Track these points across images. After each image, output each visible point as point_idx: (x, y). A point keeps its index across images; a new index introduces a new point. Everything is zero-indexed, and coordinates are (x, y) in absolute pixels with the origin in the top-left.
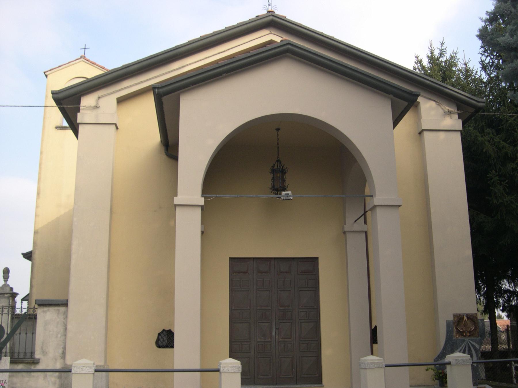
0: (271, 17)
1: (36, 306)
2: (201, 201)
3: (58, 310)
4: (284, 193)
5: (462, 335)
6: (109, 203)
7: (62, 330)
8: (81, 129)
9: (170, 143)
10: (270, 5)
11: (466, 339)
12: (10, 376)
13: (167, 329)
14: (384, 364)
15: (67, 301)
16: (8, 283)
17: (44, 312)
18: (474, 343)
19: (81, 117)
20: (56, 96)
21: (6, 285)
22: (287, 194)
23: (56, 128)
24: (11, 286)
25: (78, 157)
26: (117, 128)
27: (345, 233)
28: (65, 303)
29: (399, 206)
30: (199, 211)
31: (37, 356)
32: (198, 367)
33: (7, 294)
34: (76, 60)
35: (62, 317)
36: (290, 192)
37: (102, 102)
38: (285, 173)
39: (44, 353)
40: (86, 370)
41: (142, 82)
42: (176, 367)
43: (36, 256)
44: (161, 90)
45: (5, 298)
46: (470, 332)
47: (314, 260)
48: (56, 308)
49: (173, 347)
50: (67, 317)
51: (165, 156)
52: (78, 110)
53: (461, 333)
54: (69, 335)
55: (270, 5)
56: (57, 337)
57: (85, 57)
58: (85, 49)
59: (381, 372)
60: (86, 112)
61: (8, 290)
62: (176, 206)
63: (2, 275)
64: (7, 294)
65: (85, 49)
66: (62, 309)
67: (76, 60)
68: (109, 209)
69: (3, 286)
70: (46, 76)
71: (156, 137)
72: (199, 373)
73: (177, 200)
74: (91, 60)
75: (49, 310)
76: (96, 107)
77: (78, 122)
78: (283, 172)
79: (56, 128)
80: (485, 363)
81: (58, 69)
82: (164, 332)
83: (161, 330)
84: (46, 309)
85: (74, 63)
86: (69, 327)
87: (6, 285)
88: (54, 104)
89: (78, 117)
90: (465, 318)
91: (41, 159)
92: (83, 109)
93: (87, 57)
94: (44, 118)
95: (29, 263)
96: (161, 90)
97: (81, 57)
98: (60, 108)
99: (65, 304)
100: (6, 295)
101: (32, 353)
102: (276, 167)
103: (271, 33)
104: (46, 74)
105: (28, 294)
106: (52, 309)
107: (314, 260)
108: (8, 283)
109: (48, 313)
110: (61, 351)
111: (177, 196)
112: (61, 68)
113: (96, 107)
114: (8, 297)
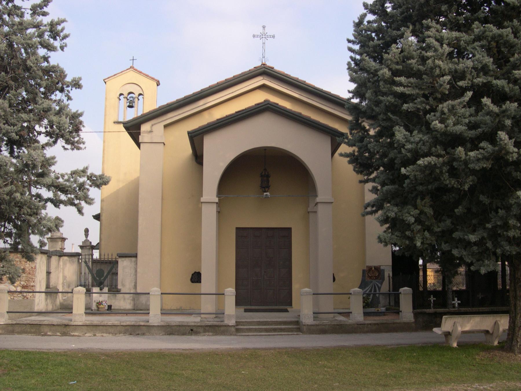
0: (264, 69)
1: (117, 257)
2: (217, 200)
3: (131, 260)
4: (265, 193)
5: (371, 278)
6: (161, 194)
7: (134, 272)
8: (141, 145)
9: (198, 154)
10: (264, 57)
11: (374, 281)
12: (108, 297)
13: (197, 271)
14: (312, 293)
15: (137, 254)
16: (88, 238)
17: (122, 261)
18: (377, 283)
19: (141, 139)
20: (126, 125)
21: (87, 241)
22: (267, 195)
23: (114, 123)
24: (90, 241)
25: (141, 165)
26: (164, 144)
27: (308, 212)
28: (135, 255)
29: (332, 203)
30: (215, 206)
31: (119, 287)
32: (214, 292)
33: (88, 246)
34: (127, 70)
35: (133, 264)
36: (268, 193)
37: (154, 128)
38: (269, 177)
39: (123, 285)
40: (157, 293)
41: (180, 114)
42: (202, 292)
43: (103, 218)
44: (192, 134)
45: (87, 249)
46: (375, 277)
47: (289, 229)
48: (130, 258)
49: (200, 282)
50: (137, 264)
51: (195, 163)
52: (139, 134)
53: (370, 277)
54: (138, 275)
55: (264, 57)
56: (131, 276)
57: (133, 67)
58: (133, 60)
59: (311, 297)
60: (144, 135)
61: (88, 244)
62: (202, 203)
63: (84, 233)
64: (88, 246)
65: (133, 60)
66: (133, 259)
67: (127, 70)
68: (161, 198)
69: (85, 241)
70: (105, 83)
71: (189, 150)
72: (215, 295)
73: (203, 199)
74: (139, 69)
75: (125, 260)
76: (151, 131)
77: (140, 141)
78: (268, 176)
79: (114, 123)
80: (394, 293)
81: (114, 77)
82: (196, 274)
83: (194, 272)
84: (123, 259)
85: (125, 72)
86: (138, 270)
87: (87, 241)
88: (124, 130)
89: (140, 138)
90: (373, 268)
91: (104, 146)
92: (143, 133)
93: (135, 67)
94: (105, 115)
95: (98, 223)
96: (192, 134)
97: (131, 68)
98: (128, 133)
99: (136, 256)
100: (87, 247)
101: (116, 285)
102: (263, 174)
103: (264, 79)
104: (105, 81)
105: (98, 243)
106: (127, 259)
107: (289, 229)
108: (88, 238)
109: (125, 262)
110: (133, 284)
111: (202, 197)
112: (116, 76)
113: (151, 131)
114: (89, 249)
